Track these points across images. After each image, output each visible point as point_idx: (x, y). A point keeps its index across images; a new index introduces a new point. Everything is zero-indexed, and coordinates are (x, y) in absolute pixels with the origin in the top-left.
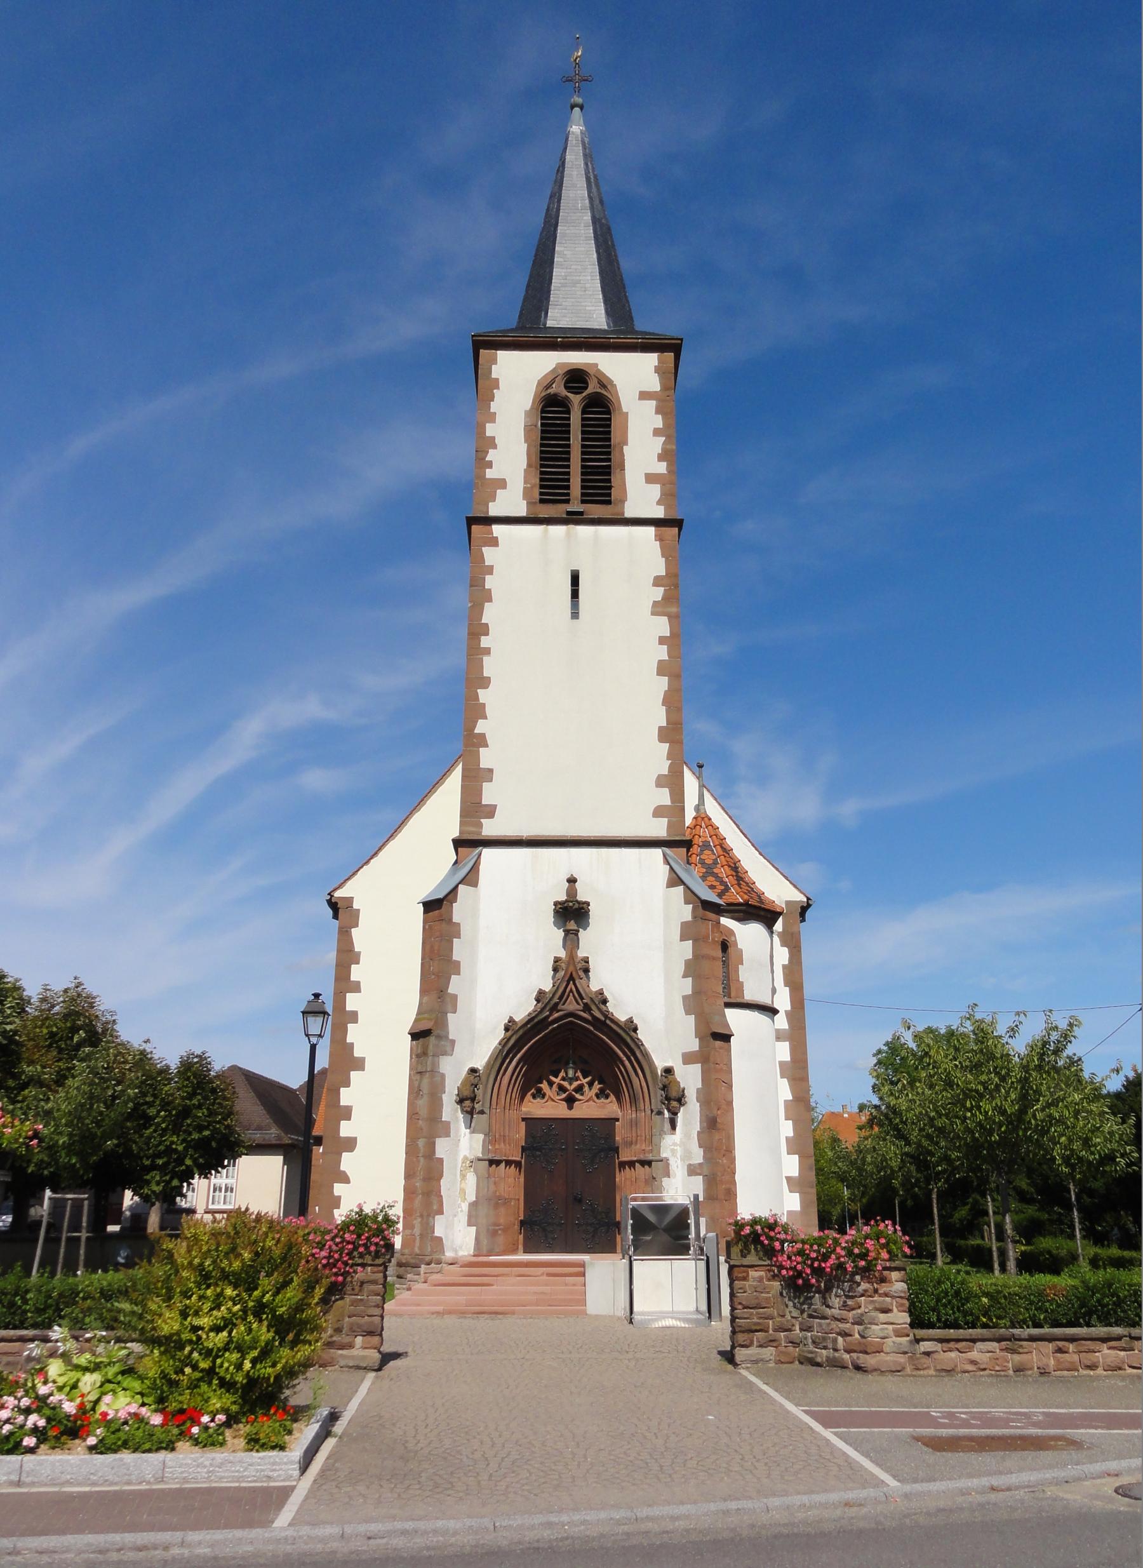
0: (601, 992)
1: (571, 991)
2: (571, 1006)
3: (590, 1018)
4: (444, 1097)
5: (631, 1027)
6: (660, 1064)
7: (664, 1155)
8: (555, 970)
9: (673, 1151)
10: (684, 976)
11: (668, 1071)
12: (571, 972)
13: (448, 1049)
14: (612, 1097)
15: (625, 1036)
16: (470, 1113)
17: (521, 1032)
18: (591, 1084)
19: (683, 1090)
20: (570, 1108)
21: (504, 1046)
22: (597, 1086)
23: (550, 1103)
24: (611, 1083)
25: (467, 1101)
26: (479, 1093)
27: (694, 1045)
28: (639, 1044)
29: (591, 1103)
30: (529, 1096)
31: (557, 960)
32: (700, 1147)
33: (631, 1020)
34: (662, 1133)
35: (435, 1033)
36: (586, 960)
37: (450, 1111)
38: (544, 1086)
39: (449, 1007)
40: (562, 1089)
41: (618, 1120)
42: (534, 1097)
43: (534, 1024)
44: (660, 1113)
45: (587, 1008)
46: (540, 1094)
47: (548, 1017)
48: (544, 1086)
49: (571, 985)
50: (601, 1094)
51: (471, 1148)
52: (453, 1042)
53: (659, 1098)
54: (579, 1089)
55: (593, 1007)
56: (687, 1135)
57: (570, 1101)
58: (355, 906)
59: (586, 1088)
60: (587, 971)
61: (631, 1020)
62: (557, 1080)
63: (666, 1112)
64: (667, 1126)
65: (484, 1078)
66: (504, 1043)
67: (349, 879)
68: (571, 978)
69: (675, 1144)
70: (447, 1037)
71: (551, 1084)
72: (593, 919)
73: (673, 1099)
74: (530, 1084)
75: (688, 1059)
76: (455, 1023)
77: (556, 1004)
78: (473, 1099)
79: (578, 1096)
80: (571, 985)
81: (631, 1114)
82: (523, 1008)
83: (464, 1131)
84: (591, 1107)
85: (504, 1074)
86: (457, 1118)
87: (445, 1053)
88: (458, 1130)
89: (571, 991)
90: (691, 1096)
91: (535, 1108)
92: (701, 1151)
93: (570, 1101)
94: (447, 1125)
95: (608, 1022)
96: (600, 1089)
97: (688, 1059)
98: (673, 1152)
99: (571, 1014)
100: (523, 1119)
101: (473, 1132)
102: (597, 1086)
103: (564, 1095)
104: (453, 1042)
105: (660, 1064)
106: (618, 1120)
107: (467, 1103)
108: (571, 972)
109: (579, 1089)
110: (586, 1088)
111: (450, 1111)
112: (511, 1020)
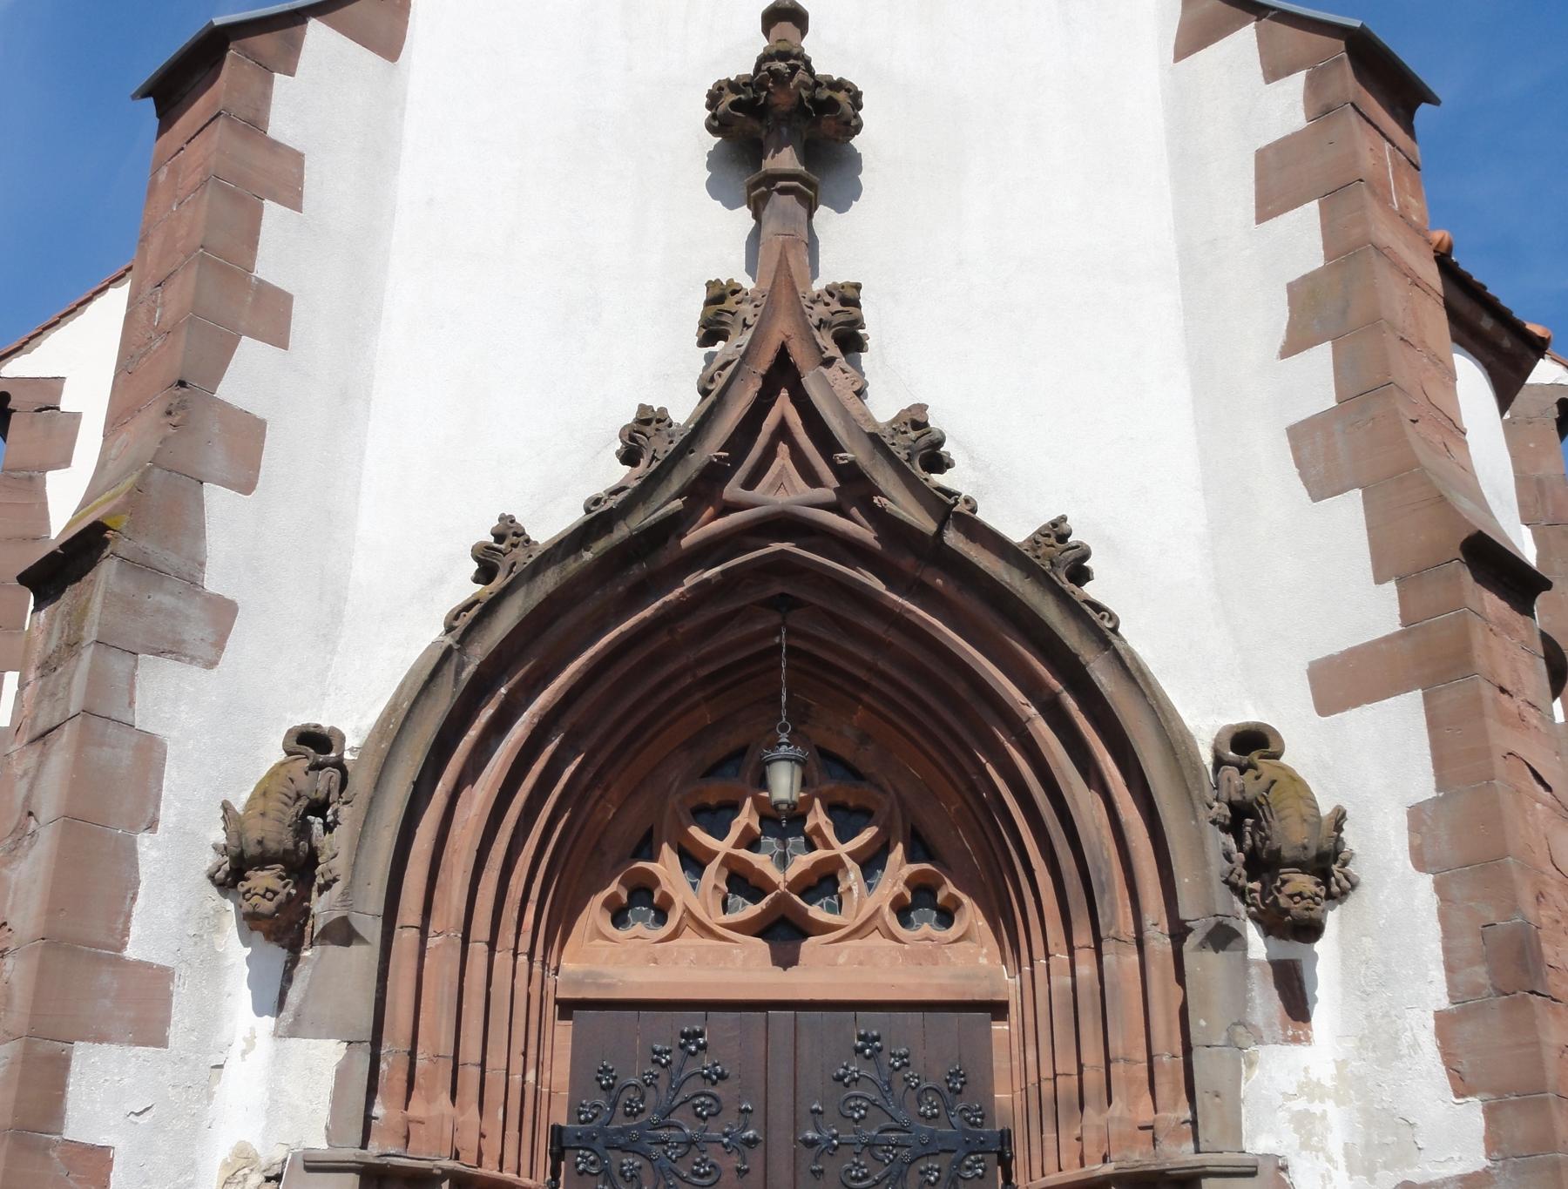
0: (915, 420)
1: (783, 431)
2: (784, 489)
3: (864, 532)
4: (148, 848)
5: (1060, 559)
6: (1204, 720)
7: (1259, 1142)
8: (711, 333)
9: (1304, 1123)
10: (1294, 345)
11: (1252, 742)
12: (782, 352)
13: (196, 632)
14: (971, 915)
15: (1033, 610)
16: (283, 930)
17: (549, 581)
18: (871, 862)
19: (1339, 818)
20: (785, 959)
21: (466, 637)
22: (898, 870)
23: (690, 940)
24: (972, 850)
25: (276, 879)
26: (335, 848)
27: (1377, 613)
28: (1099, 626)
29: (875, 940)
30: (594, 913)
31: (719, 295)
32: (1462, 1087)
33: (1057, 531)
34: (1240, 1035)
35: (120, 545)
36: (848, 297)
37: (173, 906)
38: (666, 868)
39: (217, 458)
40: (743, 882)
41: (999, 1010)
42: (619, 917)
43: (613, 556)
44: (1224, 937)
45: (855, 488)
46: (644, 899)
47: (674, 525)
48: (666, 868)
49: (784, 406)
50: (919, 901)
51: (274, 1107)
52: (223, 613)
53: (1218, 866)
54: (822, 883)
55: (884, 478)
56: (1378, 1042)
57: (784, 932)
58: (66, 405)
59: (853, 877)
60: (851, 341)
61: (1057, 531)
62: (723, 847)
63: (1253, 933)
64: (1265, 1002)
65: (361, 782)
66: (469, 622)
67: (54, 325)
68: (783, 374)
69: (1310, 1089)
70: (192, 583)
71: (693, 862)
72: (872, 140)
73: (1286, 873)
74: (591, 856)
75: (1342, 683)
76: (232, 534)
77: (715, 475)
78: (302, 867)
79: (816, 912)
80: (784, 406)
81: (1061, 967)
82: (558, 482)
83: (243, 1020)
84: (871, 955)
85: (469, 775)
86: (213, 965)
87: (172, 649)
88: (210, 1020)
89: (783, 431)
90: (1380, 846)
91: (610, 957)
92: (1472, 1115)
93: (784, 932)
94: (152, 987)
95: (953, 538)
96: (912, 882)
97: (1342, 683)
98: (1304, 1123)
99: (784, 524)
100: (567, 1008)
101: (293, 1031)
102: (898, 870)
103: (751, 910)
104: (223, 613)
105: (1204, 720)
106: (999, 1010)
107: (263, 879)
108: (782, 352)
109: (822, 883)
110: (853, 877)
111: (173, 906)
112: (508, 532)
